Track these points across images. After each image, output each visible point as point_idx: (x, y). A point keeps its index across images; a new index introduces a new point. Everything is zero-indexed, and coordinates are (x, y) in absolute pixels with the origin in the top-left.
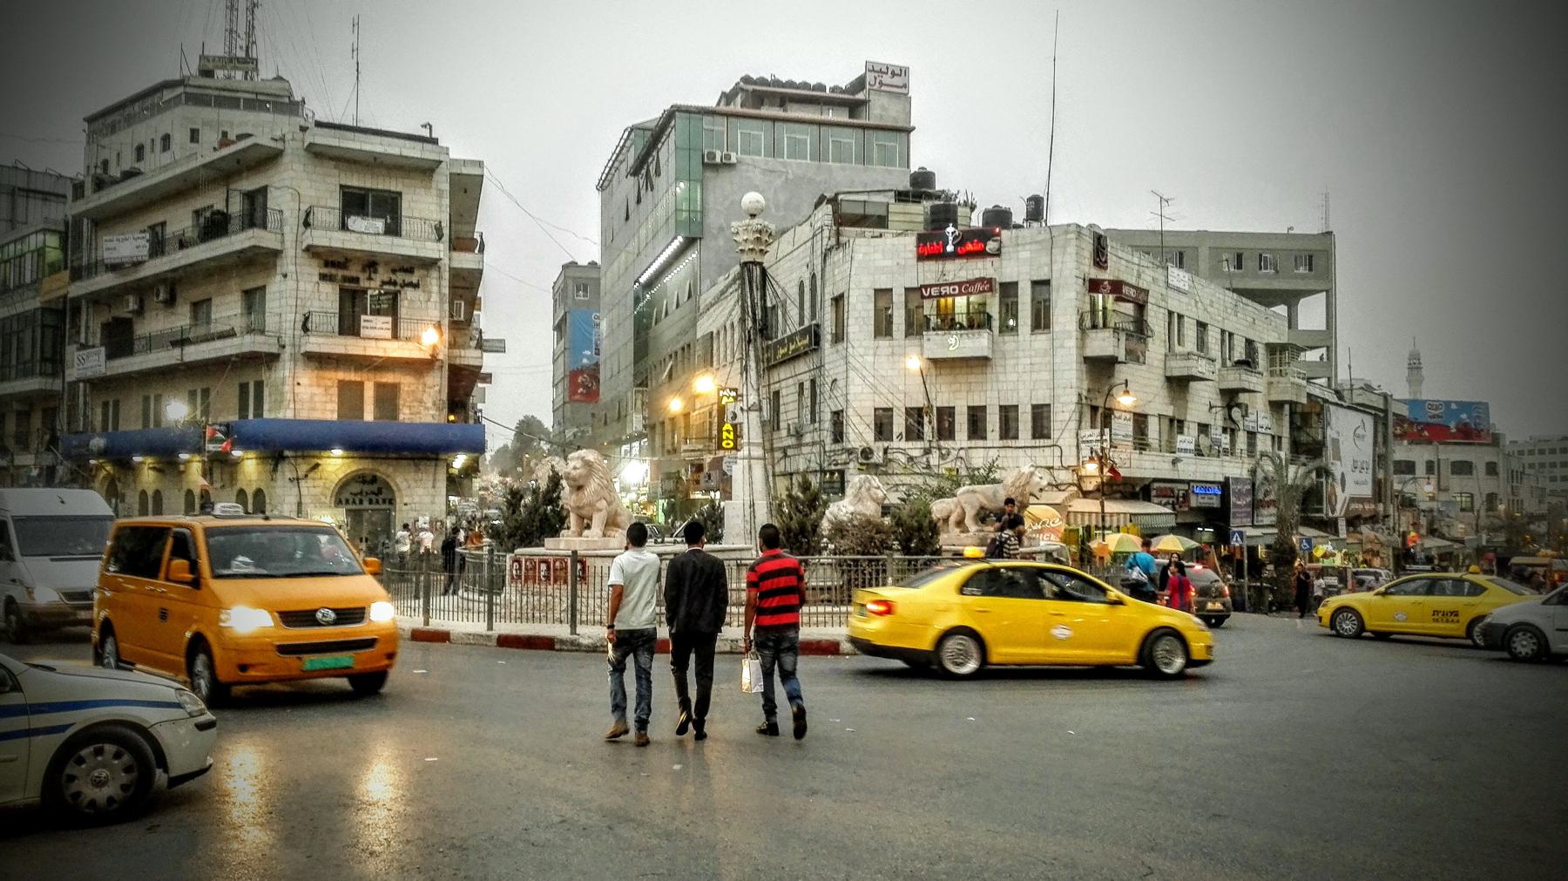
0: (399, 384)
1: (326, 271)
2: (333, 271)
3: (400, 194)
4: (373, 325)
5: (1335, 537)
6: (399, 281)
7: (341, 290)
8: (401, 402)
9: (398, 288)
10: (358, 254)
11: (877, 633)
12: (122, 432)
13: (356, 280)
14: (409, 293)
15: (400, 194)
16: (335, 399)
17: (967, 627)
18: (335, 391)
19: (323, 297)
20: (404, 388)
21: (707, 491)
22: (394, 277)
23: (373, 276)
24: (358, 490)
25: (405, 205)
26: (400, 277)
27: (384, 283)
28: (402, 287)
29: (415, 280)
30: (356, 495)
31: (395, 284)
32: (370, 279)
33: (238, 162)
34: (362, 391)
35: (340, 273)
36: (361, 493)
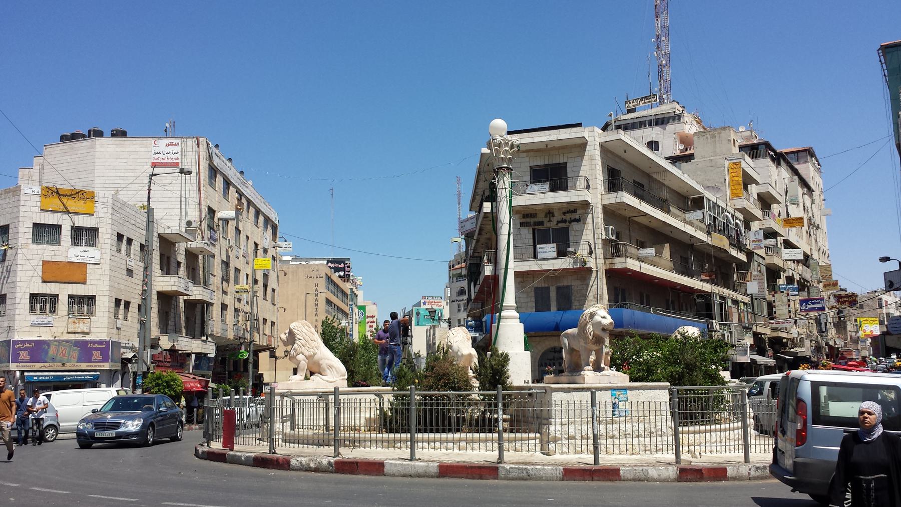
0: (571, 286)
1: (524, 220)
2: (528, 220)
3: (566, 163)
4: (544, 250)
5: (366, 430)
6: (568, 219)
7: (534, 230)
8: (573, 298)
9: (567, 224)
10: (540, 207)
11: (822, 401)
12: (260, 374)
13: (541, 223)
14: (575, 226)
15: (566, 163)
16: (533, 299)
17: (899, 387)
18: (533, 294)
19: (523, 236)
20: (574, 288)
21: (720, 329)
22: (564, 217)
23: (552, 219)
24: (552, 357)
25: (569, 170)
26: (568, 217)
27: (558, 222)
28: (570, 222)
29: (577, 217)
30: (551, 360)
31: (564, 221)
32: (550, 221)
33: (547, 146)
34: (549, 293)
35: (532, 220)
36: (554, 359)
